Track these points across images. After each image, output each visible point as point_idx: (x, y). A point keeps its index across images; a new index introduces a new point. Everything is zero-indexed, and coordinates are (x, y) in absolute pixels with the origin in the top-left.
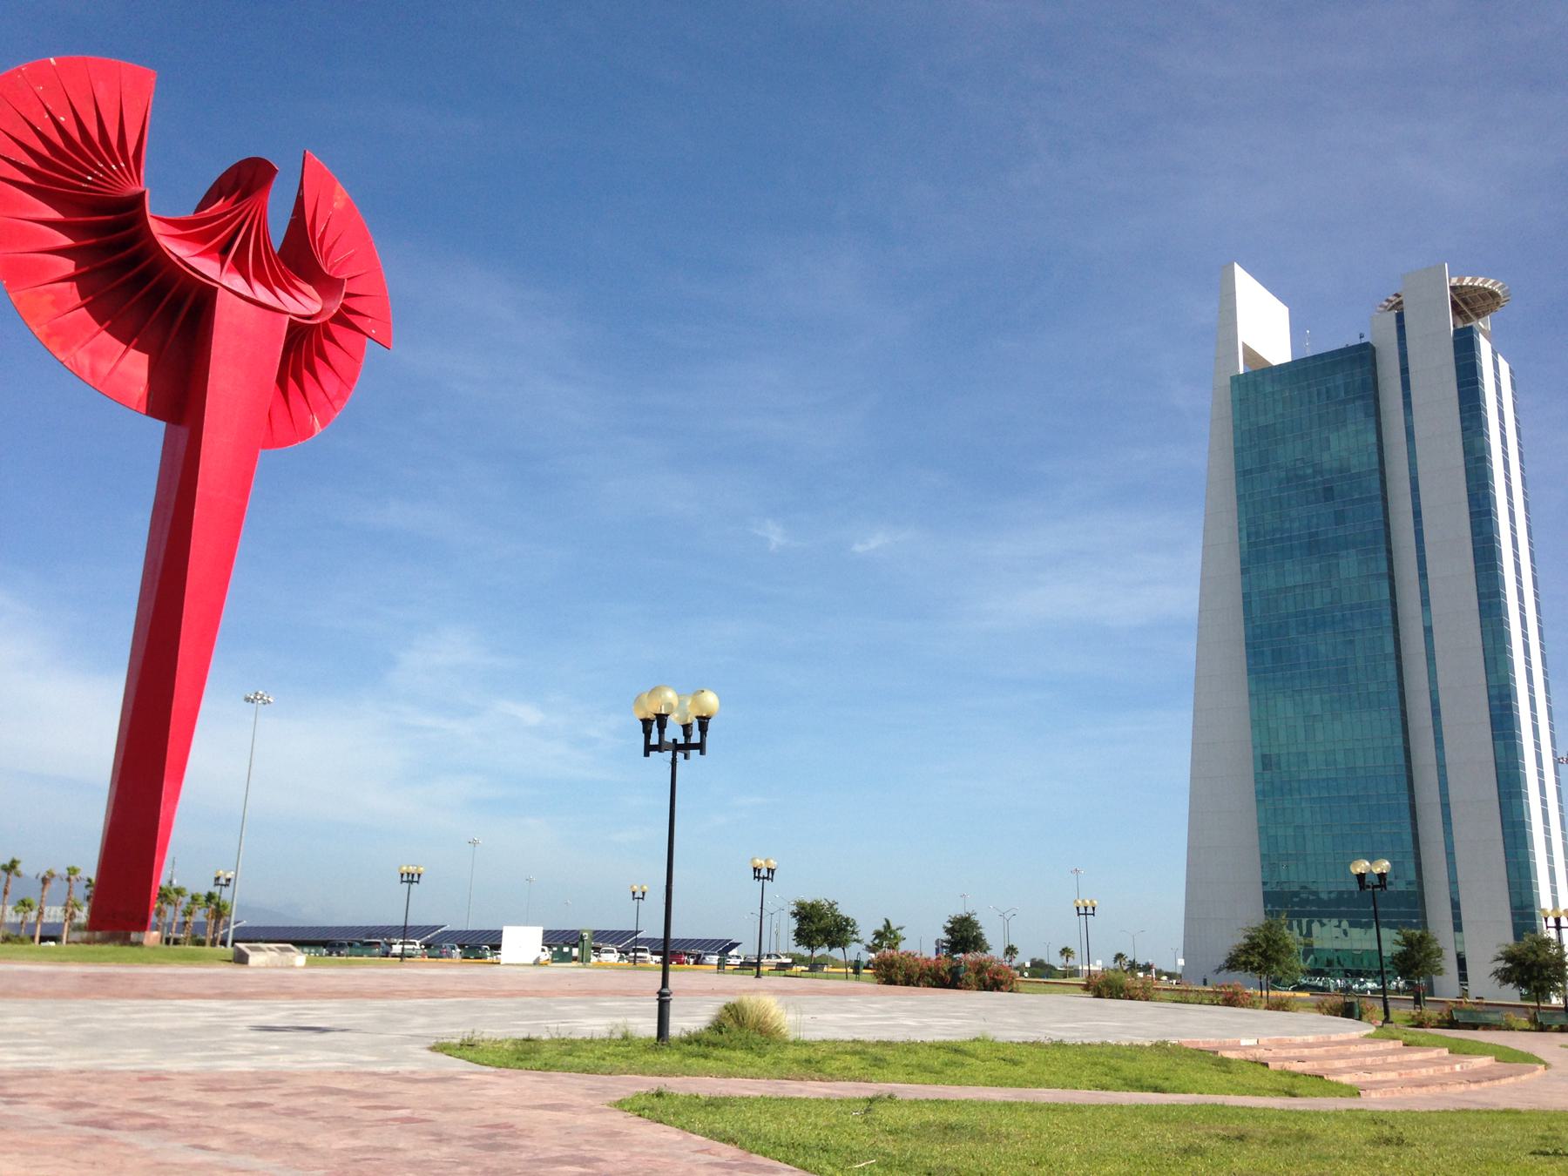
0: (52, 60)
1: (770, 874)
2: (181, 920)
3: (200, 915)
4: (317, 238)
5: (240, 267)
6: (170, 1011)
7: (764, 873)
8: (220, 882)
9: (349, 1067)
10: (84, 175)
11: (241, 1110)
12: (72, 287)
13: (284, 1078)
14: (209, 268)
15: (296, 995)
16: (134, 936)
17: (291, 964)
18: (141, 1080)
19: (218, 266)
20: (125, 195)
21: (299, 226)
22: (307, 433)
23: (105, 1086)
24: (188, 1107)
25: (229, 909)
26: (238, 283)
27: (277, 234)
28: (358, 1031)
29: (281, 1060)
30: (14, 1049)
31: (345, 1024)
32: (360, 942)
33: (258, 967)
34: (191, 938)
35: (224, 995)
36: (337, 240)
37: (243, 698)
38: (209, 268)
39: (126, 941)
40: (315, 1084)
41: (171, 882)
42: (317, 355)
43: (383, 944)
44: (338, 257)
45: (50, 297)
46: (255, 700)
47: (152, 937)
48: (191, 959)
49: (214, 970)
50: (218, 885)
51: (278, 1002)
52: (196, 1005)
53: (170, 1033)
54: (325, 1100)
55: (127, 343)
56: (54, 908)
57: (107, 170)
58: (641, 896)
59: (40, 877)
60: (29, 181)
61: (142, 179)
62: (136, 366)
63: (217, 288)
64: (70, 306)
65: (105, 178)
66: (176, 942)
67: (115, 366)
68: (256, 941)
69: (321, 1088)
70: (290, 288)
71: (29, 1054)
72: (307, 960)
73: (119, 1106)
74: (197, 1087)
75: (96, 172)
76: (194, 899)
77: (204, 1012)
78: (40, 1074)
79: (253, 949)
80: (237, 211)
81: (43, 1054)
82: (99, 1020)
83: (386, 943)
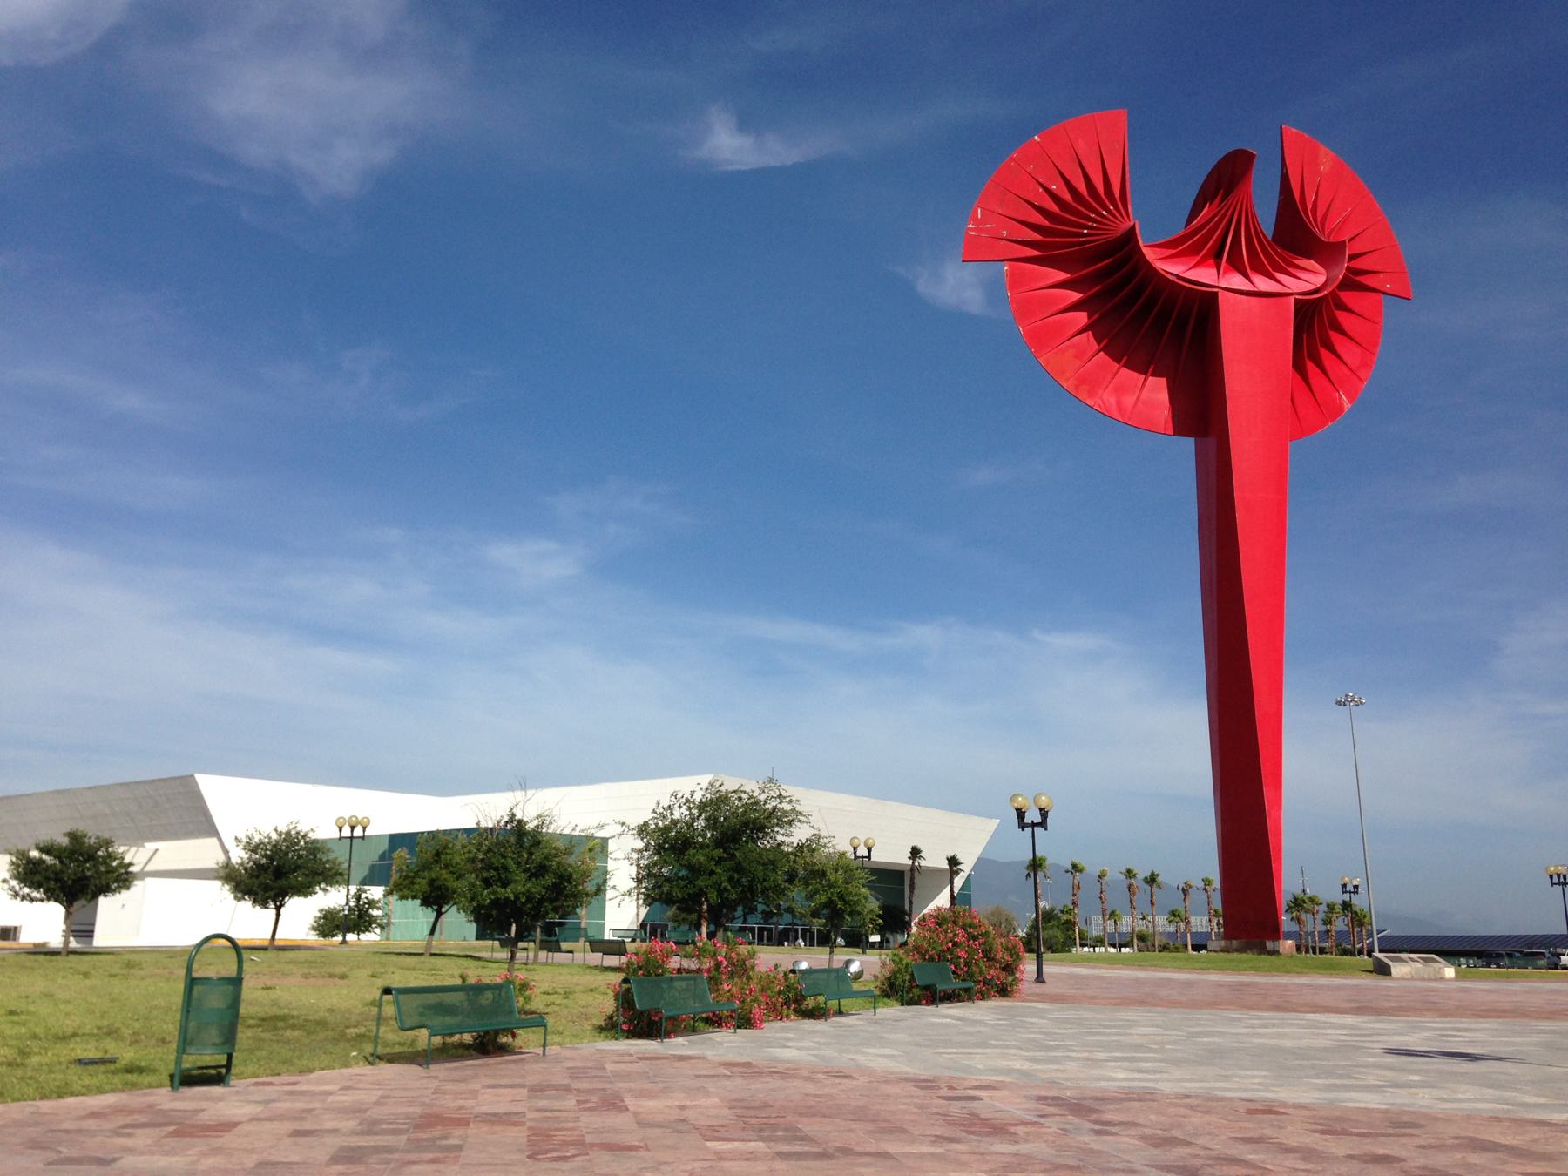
0: (1036, 137)
2: (1323, 928)
3: (1340, 924)
4: (1309, 210)
5: (1236, 266)
6: (1299, 1026)
8: (1348, 890)
9: (1508, 1111)
10: (1080, 230)
11: (1363, 1166)
12: (1088, 336)
13: (1422, 1122)
14: (1205, 275)
15: (1444, 1013)
16: (1269, 945)
17: (1439, 976)
18: (1250, 1112)
19: (1214, 271)
20: (1119, 235)
21: (1289, 206)
22: (1337, 411)
23: (1207, 1118)
24: (1297, 1155)
25: (1368, 917)
26: (1236, 281)
27: (1266, 216)
28: (1522, 1061)
29: (1421, 1095)
30: (1126, 1064)
31: (1502, 1050)
32: (1521, 952)
33: (1403, 979)
34: (1337, 946)
35: (1360, 1010)
36: (1330, 206)
37: (1334, 702)
38: (1205, 275)
39: (1262, 950)
40: (1463, 1134)
41: (1304, 891)
42: (1331, 330)
43: (1548, 955)
44: (1334, 222)
45: (1072, 351)
46: (1346, 703)
47: (1287, 945)
48: (1331, 969)
49: (1354, 981)
50: (1346, 892)
51: (1423, 1019)
52: (1329, 1020)
53: (1297, 1053)
54: (1475, 1158)
55: (1145, 373)
56: (1199, 919)
57: (1099, 218)
58: (1038, 819)
59: (1180, 888)
60: (1037, 253)
61: (1131, 215)
62: (1157, 392)
63: (1217, 293)
64: (1091, 353)
65: (1099, 226)
66: (1322, 951)
67: (1138, 398)
68: (1400, 951)
69: (1471, 1139)
70: (1291, 270)
71: (1140, 1071)
72: (1456, 972)
73: (1218, 1147)
74: (1314, 1127)
75: (1090, 224)
76: (1331, 907)
77: (1336, 1029)
78: (1145, 1097)
79: (1392, 959)
80: (1223, 212)
81: (1155, 1072)
82: (1221, 1034)
83: (1553, 954)
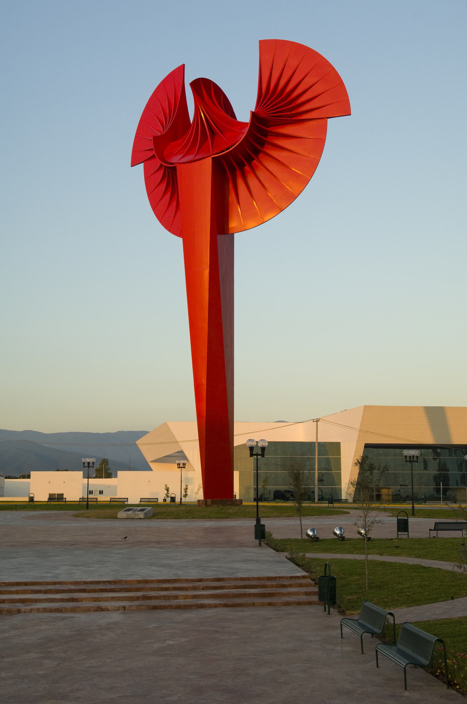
1: (184, 466)
7: (181, 465)
